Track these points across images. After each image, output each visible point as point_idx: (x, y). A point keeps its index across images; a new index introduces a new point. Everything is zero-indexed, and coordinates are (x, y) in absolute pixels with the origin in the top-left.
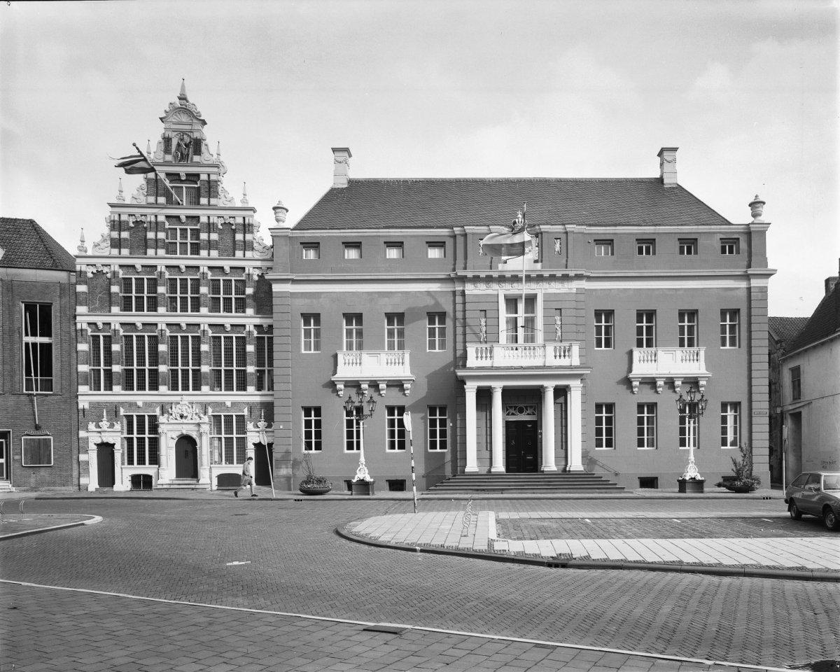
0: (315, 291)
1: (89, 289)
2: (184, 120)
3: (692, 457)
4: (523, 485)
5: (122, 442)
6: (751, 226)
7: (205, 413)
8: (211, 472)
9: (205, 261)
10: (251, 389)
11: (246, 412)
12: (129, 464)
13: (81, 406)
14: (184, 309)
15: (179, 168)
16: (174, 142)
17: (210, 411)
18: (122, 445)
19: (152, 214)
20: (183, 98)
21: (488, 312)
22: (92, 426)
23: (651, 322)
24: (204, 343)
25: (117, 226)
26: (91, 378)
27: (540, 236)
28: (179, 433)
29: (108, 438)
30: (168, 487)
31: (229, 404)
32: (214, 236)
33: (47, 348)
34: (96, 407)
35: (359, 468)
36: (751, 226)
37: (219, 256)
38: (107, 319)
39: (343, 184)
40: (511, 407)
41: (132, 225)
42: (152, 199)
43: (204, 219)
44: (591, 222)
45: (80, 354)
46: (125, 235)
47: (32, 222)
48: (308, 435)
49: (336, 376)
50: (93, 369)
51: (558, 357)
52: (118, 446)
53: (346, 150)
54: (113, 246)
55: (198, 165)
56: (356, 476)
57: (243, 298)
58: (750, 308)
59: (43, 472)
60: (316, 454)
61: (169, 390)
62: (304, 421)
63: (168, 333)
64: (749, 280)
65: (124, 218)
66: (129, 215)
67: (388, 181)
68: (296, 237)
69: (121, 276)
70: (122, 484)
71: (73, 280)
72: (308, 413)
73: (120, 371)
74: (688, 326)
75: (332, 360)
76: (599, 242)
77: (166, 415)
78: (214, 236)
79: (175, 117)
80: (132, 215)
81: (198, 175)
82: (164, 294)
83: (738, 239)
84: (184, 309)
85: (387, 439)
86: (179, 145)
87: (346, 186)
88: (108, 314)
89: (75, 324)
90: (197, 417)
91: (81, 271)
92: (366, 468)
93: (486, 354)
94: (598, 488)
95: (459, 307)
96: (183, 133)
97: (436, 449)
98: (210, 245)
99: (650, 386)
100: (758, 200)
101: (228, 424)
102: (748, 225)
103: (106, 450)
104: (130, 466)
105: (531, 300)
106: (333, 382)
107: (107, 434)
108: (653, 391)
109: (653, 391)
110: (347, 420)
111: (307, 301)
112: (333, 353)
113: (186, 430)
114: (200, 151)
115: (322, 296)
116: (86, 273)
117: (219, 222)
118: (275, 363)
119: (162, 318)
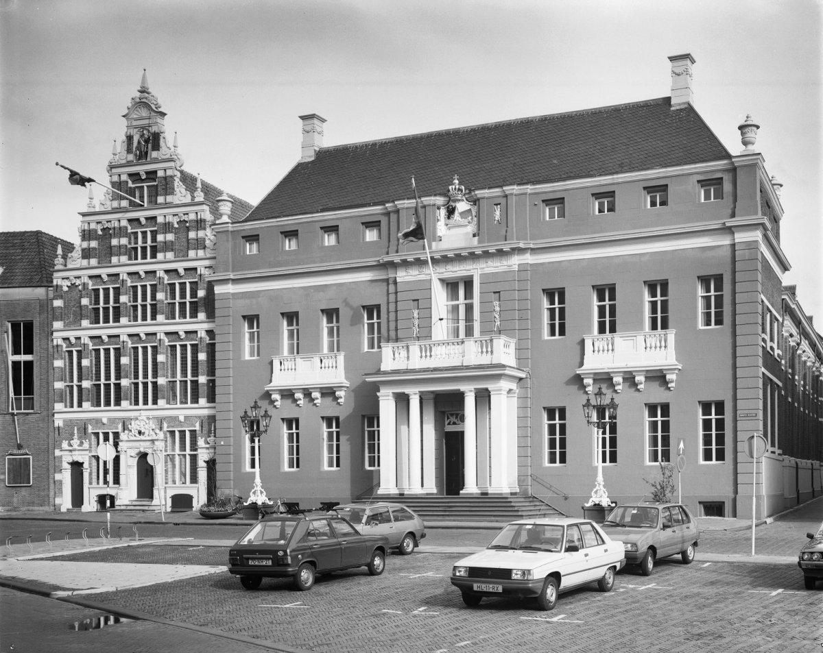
1: (65, 303)
2: (144, 115)
5: (90, 461)
7: (161, 429)
8: (165, 492)
9: (163, 263)
10: (203, 401)
11: (197, 428)
12: (192, 483)
13: (56, 425)
14: (183, 315)
15: (145, 165)
16: (136, 139)
17: (165, 425)
18: (90, 464)
19: (115, 219)
20: (143, 91)
21: (422, 302)
22: (65, 445)
24: (161, 353)
25: (87, 236)
26: (131, 393)
27: (477, 203)
28: (137, 451)
29: (78, 458)
30: (123, 508)
31: (105, 421)
32: (170, 237)
33: (29, 365)
34: (69, 424)
35: (595, 490)
38: (78, 333)
39: (310, 157)
40: (452, 415)
41: (100, 233)
42: (115, 204)
43: (160, 220)
44: (346, 205)
45: (56, 370)
46: (94, 244)
47: (38, 234)
48: (707, 440)
49: (583, 368)
50: (68, 386)
51: (424, 358)
52: (86, 465)
53: (687, 57)
54: (84, 257)
55: (156, 161)
56: (591, 501)
57: (196, 301)
59: (24, 492)
61: (131, 404)
62: (546, 426)
63: (130, 345)
65: (93, 226)
66: (174, 215)
67: (356, 147)
68: (238, 231)
69: (90, 287)
70: (90, 505)
71: (51, 295)
72: (706, 411)
73: (90, 387)
74: (661, 301)
75: (578, 348)
76: (547, 202)
77: (126, 432)
78: (170, 237)
79: (137, 111)
80: (176, 215)
81: (155, 172)
82: (87, 306)
84: (183, 315)
85: (701, 447)
87: (313, 159)
88: (78, 328)
89: (52, 340)
90: (153, 433)
91: (57, 285)
93: (487, 348)
94: (494, 516)
95: (392, 298)
96: (143, 128)
98: (167, 247)
100: (748, 123)
101: (185, 438)
103: (77, 466)
104: (193, 485)
105: (468, 283)
107: (77, 453)
109: (582, 391)
110: (704, 420)
111: (248, 301)
113: (143, 447)
114: (159, 146)
115: (261, 295)
116: (61, 287)
117: (175, 221)
118: (218, 372)
119: (124, 329)
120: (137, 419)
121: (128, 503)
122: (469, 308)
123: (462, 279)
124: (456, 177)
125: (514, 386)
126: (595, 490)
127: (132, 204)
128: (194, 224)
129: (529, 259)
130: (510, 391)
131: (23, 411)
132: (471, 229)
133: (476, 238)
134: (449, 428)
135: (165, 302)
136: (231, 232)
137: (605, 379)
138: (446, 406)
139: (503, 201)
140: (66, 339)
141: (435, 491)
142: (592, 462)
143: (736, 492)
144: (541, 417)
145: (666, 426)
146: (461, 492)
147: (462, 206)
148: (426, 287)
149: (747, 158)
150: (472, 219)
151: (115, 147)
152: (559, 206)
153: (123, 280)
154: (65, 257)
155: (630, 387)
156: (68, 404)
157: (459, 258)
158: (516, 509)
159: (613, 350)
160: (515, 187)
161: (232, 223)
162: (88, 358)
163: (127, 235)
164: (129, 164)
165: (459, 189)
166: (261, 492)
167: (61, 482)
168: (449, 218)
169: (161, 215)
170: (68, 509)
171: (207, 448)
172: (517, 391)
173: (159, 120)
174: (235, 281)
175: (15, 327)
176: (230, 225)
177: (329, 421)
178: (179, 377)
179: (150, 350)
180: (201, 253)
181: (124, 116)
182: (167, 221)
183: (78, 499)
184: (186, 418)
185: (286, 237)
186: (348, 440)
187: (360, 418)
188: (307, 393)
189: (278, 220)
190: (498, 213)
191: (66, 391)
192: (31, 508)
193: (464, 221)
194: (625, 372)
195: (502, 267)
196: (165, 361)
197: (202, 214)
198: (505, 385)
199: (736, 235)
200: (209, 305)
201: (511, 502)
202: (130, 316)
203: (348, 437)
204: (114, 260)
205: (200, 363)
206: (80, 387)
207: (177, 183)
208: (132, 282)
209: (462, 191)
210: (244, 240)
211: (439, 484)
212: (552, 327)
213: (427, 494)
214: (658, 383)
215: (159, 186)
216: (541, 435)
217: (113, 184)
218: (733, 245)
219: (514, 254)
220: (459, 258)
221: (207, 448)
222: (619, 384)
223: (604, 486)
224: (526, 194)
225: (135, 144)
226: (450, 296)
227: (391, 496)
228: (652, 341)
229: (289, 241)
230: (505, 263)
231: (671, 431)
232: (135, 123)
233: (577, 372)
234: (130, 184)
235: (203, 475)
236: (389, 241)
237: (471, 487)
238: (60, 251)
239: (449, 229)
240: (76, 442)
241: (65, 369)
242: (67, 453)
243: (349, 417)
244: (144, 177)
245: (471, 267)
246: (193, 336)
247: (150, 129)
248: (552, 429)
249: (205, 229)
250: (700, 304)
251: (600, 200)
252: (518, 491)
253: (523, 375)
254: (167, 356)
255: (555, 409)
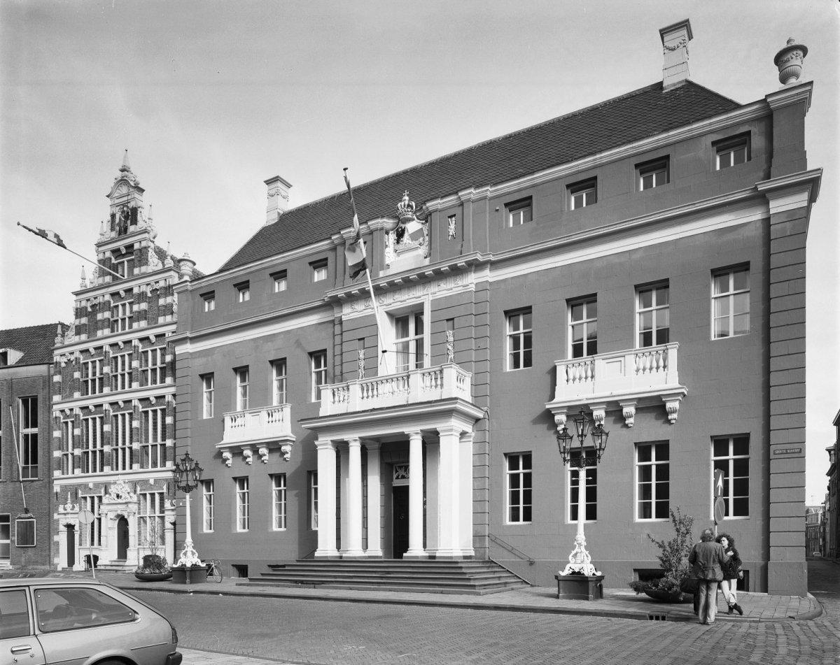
0: (201, 349)
3: (581, 536)
4: (389, 573)
6: (769, 100)
11: (165, 490)
13: (55, 491)
17: (138, 488)
22: (61, 509)
23: (245, 381)
28: (115, 514)
30: (103, 568)
31: (91, 485)
32: (144, 306)
33: (35, 436)
34: (65, 488)
35: (574, 552)
36: (769, 100)
37: (148, 325)
40: (400, 467)
49: (555, 401)
56: (568, 566)
58: (768, 255)
59: (30, 552)
60: (524, 525)
64: (766, 203)
65: (84, 304)
70: (80, 565)
71: (52, 371)
72: (645, 455)
75: (548, 378)
77: (107, 496)
78: (144, 306)
83: (749, 133)
85: (637, 501)
86: (120, 219)
92: (585, 552)
97: (650, 517)
99: (613, 418)
100: (186, 258)
102: (764, 101)
103: (70, 527)
105: (418, 313)
106: (549, 411)
108: (553, 431)
109: (553, 431)
112: (549, 367)
116: (60, 363)
117: (148, 290)
120: (115, 483)
121: (109, 563)
122: (420, 344)
123: (412, 312)
124: (406, 193)
125: (468, 428)
126: (574, 552)
127: (115, 278)
128: (163, 291)
129: (488, 275)
130: (463, 434)
131: (30, 479)
132: (423, 251)
133: (428, 259)
134: (397, 483)
135: (140, 369)
136: (191, 291)
137: (581, 414)
138: (390, 456)
139: (458, 211)
140: (62, 411)
141: (380, 553)
142: (633, 518)
143: (767, 556)
144: (501, 465)
145: (663, 472)
146: (404, 554)
147: (413, 226)
148: (371, 323)
149: (211, 278)
150: (424, 240)
151: (102, 227)
152: (588, 190)
153: (106, 352)
154: (63, 336)
155: (615, 422)
156: (115, 467)
157: (408, 283)
158: (467, 577)
159: (592, 377)
160: (472, 190)
161: (191, 282)
162: (79, 427)
163: (110, 309)
164: (112, 241)
165: (409, 205)
166: (193, 554)
167: (58, 543)
168: (398, 243)
169: (138, 287)
170: (63, 568)
171: (172, 510)
172: (473, 434)
173: (136, 195)
174: (193, 340)
175: (25, 402)
176: (188, 283)
177: (277, 478)
178: (151, 441)
179: (159, 413)
180: (169, 318)
181: (108, 196)
182: (141, 290)
183: (71, 561)
184: (156, 481)
185: (641, 173)
186: (296, 495)
187: (305, 474)
188: (254, 448)
189: (230, 272)
190: (452, 226)
191: (63, 459)
192: (35, 567)
193: (416, 244)
194: (609, 403)
195: (457, 289)
196: (60, 436)
197: (170, 279)
198: (457, 424)
199: (772, 204)
200: (170, 369)
201: (461, 568)
202: (112, 385)
203: (297, 491)
204: (99, 333)
205: (167, 426)
206: (130, 448)
207: (151, 253)
208: (113, 353)
209: (412, 207)
210: (202, 299)
211: (385, 546)
212: (516, 357)
213: (370, 557)
214: (653, 415)
215: (135, 255)
216: (501, 486)
217: (100, 261)
218: (767, 222)
219: (471, 271)
220: (408, 283)
221: (172, 510)
222: (631, 417)
223: (586, 548)
224: (485, 198)
225: (117, 221)
226: (400, 332)
227: (329, 559)
228: (646, 361)
229: (243, 294)
230: (460, 283)
231: (533, 485)
232: (117, 201)
233: (547, 407)
234: (114, 261)
235: (169, 536)
236: (336, 278)
237: (416, 549)
238: (59, 331)
239: (399, 254)
240: (69, 506)
241: (63, 439)
242: (65, 515)
243: (296, 473)
244: (124, 252)
245: (407, 297)
246: (161, 400)
247: (129, 205)
248: (514, 480)
249: (173, 295)
250: (508, 344)
251: (578, 194)
252: (473, 554)
253: (480, 415)
254: (141, 422)
255: (519, 456)
